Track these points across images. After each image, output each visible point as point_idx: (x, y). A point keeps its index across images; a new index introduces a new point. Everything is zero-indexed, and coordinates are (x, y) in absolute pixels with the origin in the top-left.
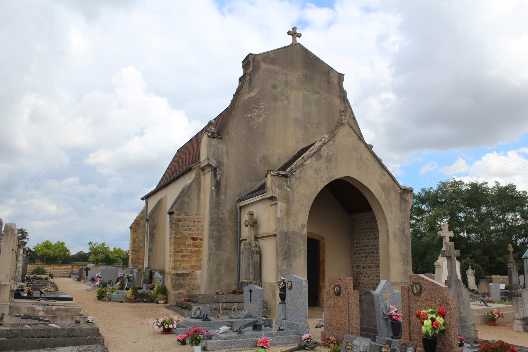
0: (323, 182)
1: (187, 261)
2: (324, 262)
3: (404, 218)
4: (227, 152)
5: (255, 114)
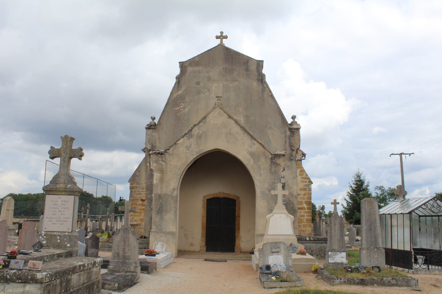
0: (193, 155)
1: (138, 216)
2: (239, 217)
5: (182, 107)
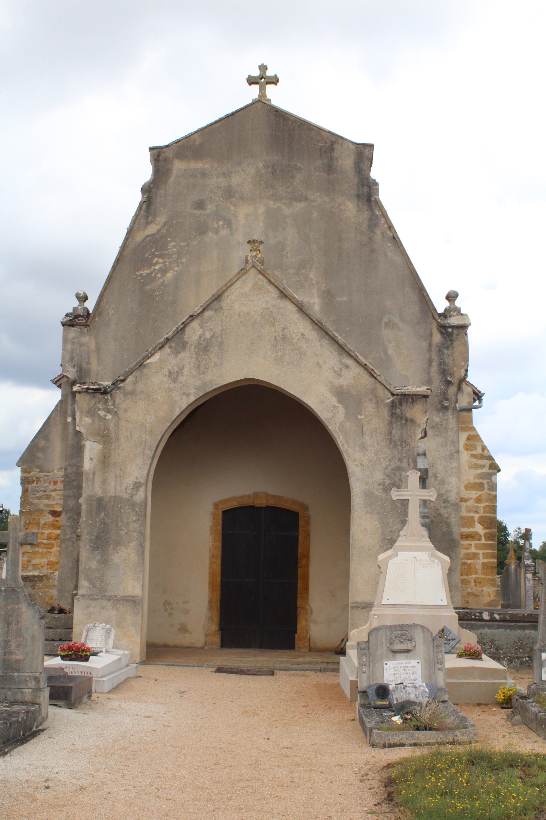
0: (188, 395)
1: (42, 553)
3: (400, 460)
4: (98, 349)
5: (157, 267)
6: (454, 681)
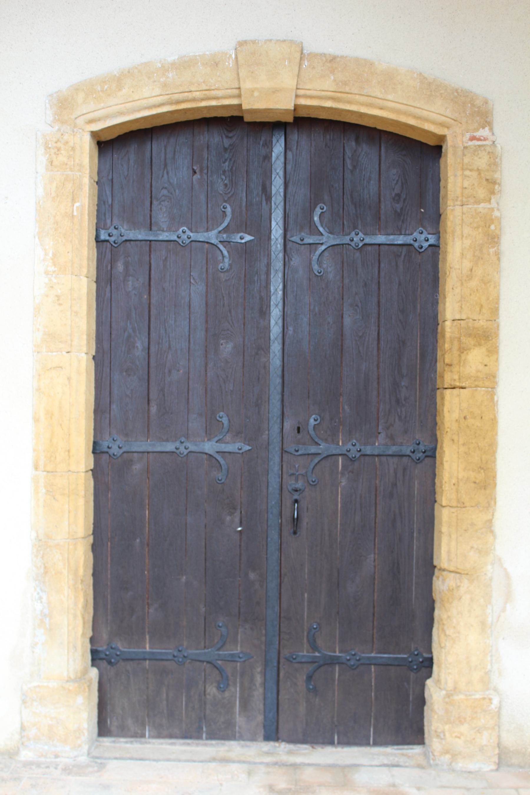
6: (339, 518)
